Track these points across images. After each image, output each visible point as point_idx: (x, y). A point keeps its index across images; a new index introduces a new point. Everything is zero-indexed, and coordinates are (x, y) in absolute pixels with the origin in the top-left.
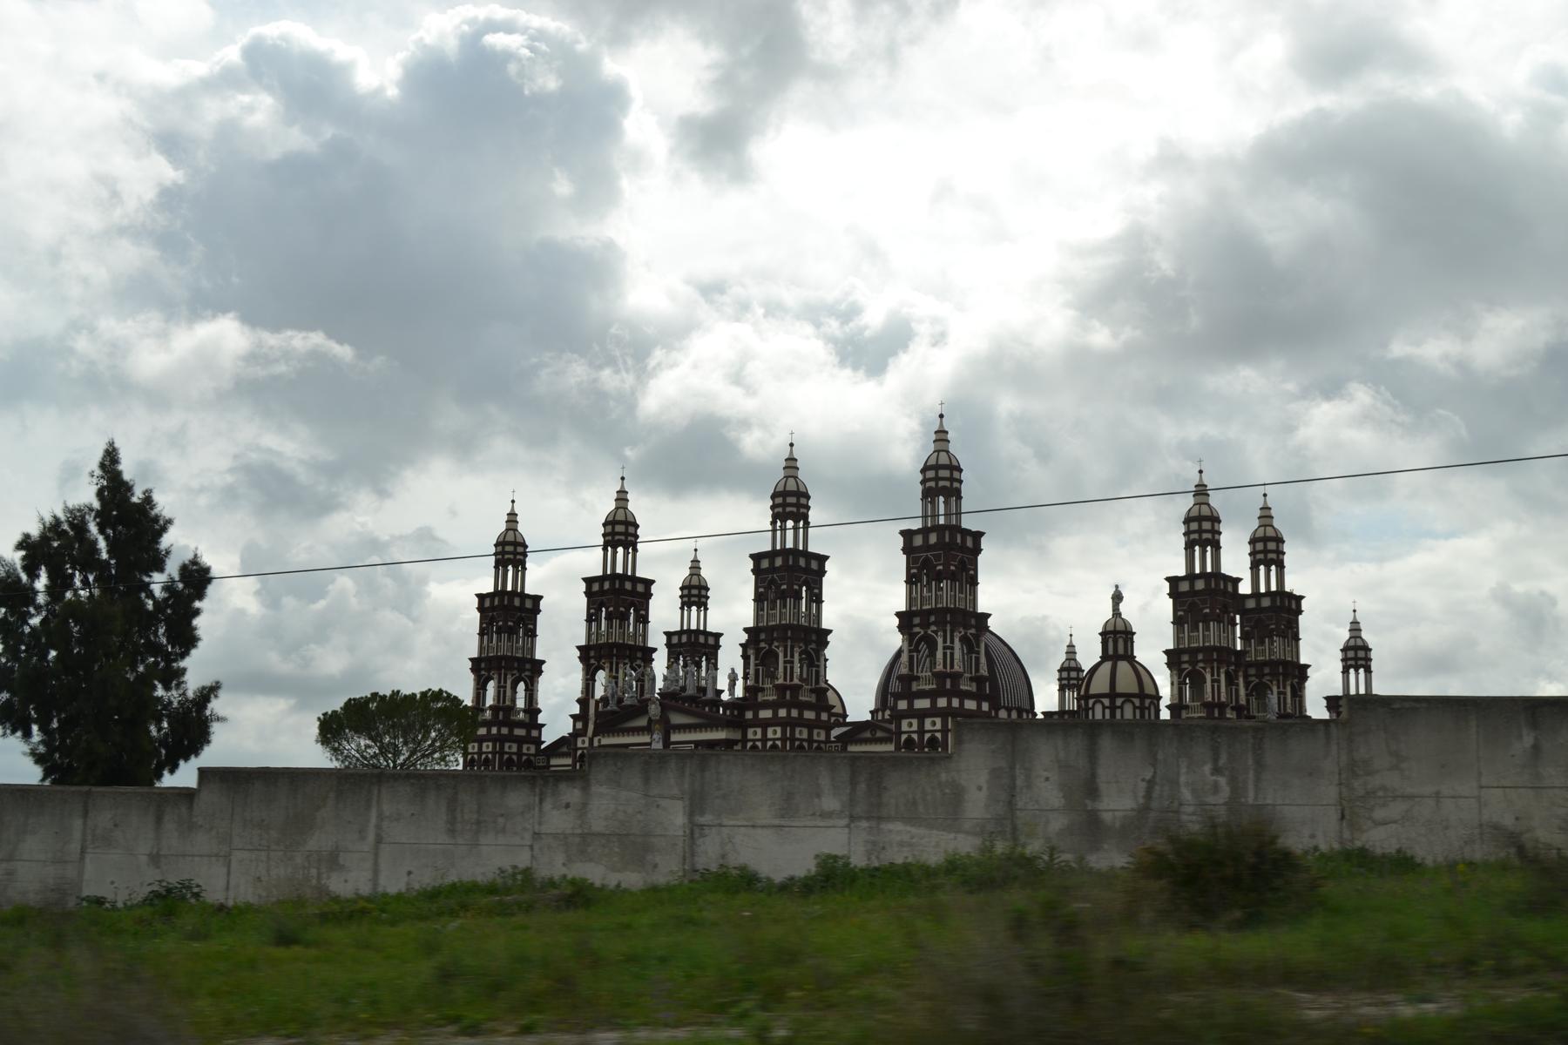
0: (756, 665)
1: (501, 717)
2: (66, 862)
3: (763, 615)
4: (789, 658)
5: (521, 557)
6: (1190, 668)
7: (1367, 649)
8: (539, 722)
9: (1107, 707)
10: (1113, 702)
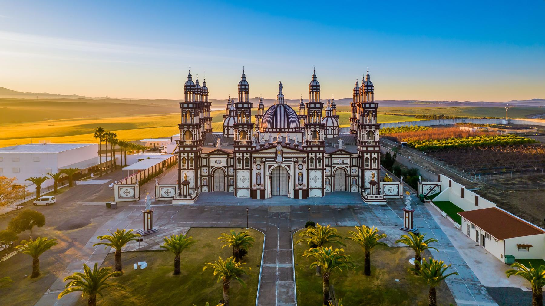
5: (247, 90)
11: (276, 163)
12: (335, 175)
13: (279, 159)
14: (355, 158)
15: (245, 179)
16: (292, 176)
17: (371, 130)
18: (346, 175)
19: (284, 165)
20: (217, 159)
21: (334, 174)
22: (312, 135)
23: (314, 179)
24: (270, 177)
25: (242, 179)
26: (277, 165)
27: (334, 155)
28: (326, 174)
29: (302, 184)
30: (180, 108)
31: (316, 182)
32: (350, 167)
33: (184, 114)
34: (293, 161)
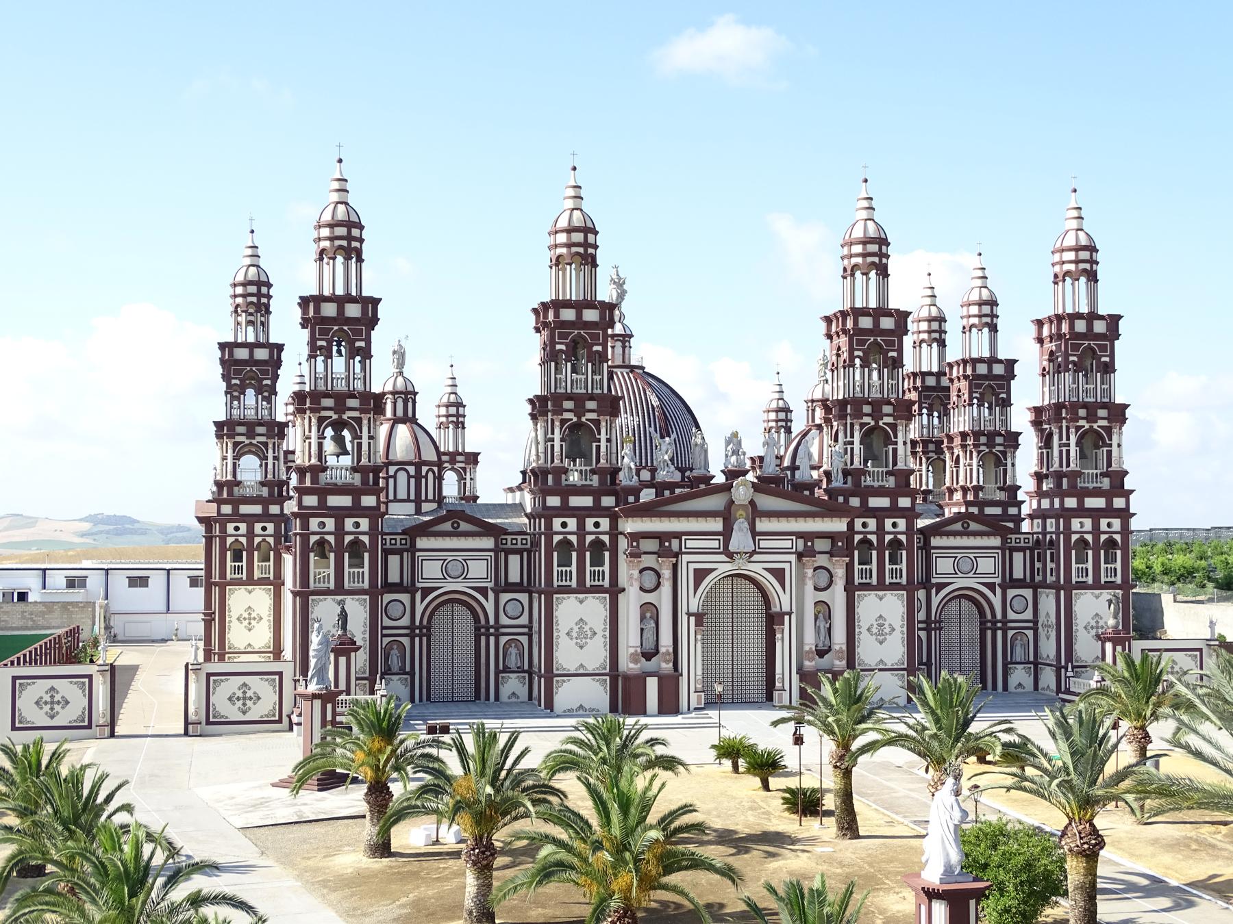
1: (1065, 486)
2: (871, 713)
4: (849, 439)
9: (412, 477)
10: (418, 470)
11: (723, 558)
12: (429, 629)
13: (740, 539)
14: (519, 552)
15: (589, 633)
16: (790, 614)
17: (1095, 426)
18: (477, 629)
19: (756, 569)
21: (425, 622)
22: (564, 443)
23: (874, 630)
24: (700, 618)
25: (574, 634)
26: (728, 567)
27: (425, 539)
28: (387, 622)
29: (830, 649)
30: (303, 327)
31: (881, 643)
32: (1004, 587)
33: (561, 351)
34: (794, 550)
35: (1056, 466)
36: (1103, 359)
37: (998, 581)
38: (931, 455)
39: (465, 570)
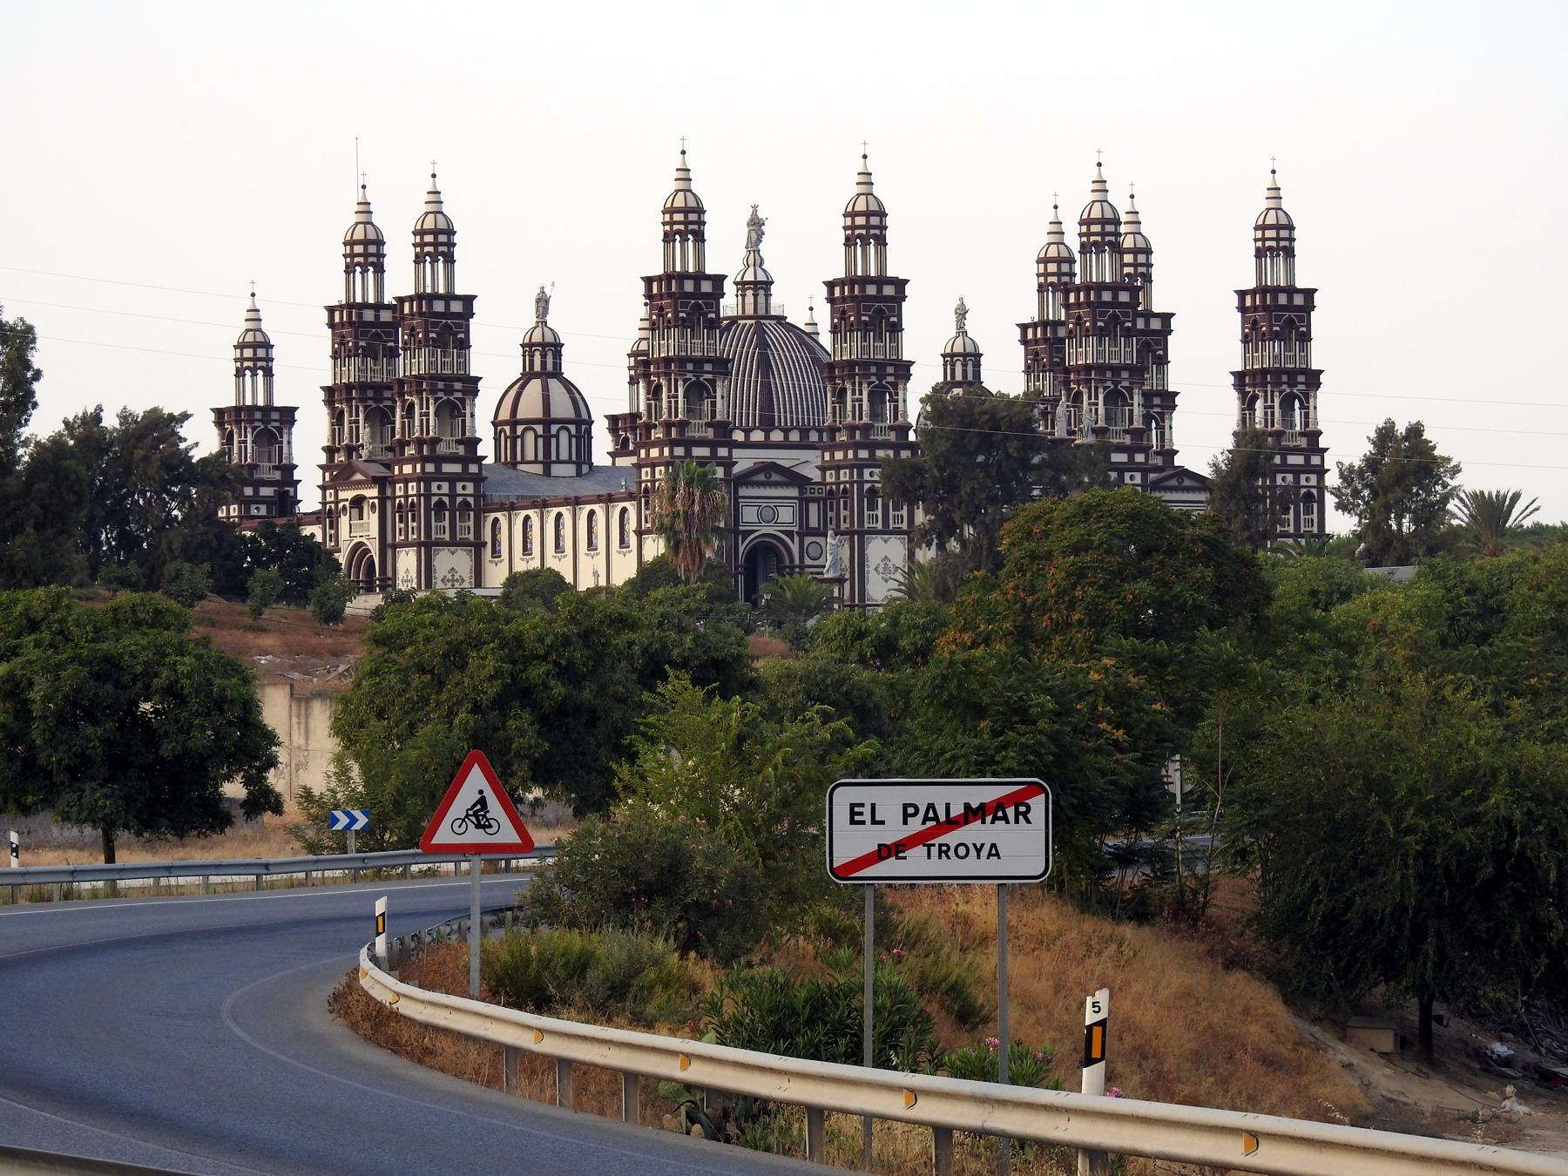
0: (833, 403)
3: (846, 348)
6: (1112, 387)
7: (267, 346)
8: (1320, 446)
9: (540, 436)
10: (547, 430)
14: (816, 500)
20: (764, 502)
25: (881, 570)
32: (802, 536)
35: (665, 417)
36: (1301, 329)
37: (796, 529)
38: (370, 403)
39: (775, 515)
